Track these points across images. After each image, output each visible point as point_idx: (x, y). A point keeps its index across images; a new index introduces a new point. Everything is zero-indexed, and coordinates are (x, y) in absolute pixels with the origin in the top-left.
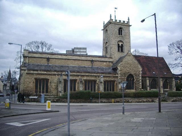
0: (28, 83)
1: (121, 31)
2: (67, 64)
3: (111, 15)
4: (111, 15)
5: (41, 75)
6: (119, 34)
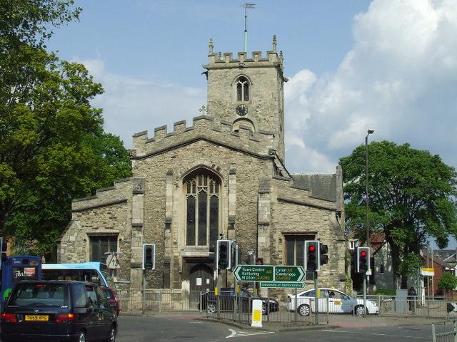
1: (247, 86)
6: (240, 99)
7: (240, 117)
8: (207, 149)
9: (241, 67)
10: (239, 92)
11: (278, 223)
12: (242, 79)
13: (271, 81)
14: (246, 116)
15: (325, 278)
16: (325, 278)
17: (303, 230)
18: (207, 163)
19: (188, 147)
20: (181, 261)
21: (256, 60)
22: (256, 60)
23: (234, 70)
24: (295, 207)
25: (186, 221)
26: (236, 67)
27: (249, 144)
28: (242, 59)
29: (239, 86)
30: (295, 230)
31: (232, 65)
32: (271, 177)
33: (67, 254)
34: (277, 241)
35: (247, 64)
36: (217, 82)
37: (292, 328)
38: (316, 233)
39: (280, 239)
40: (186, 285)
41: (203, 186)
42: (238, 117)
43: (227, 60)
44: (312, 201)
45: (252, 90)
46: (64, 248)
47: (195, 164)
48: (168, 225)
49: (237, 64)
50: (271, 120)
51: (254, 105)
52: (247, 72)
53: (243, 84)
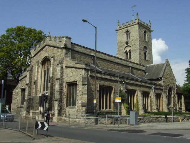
9: (127, 27)
10: (127, 37)
12: (128, 31)
13: (136, 30)
14: (128, 45)
15: (80, 105)
16: (80, 105)
18: (47, 55)
19: (43, 50)
21: (131, 24)
22: (131, 24)
23: (125, 29)
24: (70, 69)
26: (125, 28)
27: (59, 44)
28: (127, 24)
31: (124, 27)
32: (64, 56)
34: (65, 87)
35: (129, 26)
36: (120, 35)
38: (77, 81)
40: (41, 109)
42: (126, 45)
43: (122, 26)
44: (78, 66)
46: (14, 94)
47: (44, 57)
49: (126, 27)
50: (137, 44)
51: (131, 40)
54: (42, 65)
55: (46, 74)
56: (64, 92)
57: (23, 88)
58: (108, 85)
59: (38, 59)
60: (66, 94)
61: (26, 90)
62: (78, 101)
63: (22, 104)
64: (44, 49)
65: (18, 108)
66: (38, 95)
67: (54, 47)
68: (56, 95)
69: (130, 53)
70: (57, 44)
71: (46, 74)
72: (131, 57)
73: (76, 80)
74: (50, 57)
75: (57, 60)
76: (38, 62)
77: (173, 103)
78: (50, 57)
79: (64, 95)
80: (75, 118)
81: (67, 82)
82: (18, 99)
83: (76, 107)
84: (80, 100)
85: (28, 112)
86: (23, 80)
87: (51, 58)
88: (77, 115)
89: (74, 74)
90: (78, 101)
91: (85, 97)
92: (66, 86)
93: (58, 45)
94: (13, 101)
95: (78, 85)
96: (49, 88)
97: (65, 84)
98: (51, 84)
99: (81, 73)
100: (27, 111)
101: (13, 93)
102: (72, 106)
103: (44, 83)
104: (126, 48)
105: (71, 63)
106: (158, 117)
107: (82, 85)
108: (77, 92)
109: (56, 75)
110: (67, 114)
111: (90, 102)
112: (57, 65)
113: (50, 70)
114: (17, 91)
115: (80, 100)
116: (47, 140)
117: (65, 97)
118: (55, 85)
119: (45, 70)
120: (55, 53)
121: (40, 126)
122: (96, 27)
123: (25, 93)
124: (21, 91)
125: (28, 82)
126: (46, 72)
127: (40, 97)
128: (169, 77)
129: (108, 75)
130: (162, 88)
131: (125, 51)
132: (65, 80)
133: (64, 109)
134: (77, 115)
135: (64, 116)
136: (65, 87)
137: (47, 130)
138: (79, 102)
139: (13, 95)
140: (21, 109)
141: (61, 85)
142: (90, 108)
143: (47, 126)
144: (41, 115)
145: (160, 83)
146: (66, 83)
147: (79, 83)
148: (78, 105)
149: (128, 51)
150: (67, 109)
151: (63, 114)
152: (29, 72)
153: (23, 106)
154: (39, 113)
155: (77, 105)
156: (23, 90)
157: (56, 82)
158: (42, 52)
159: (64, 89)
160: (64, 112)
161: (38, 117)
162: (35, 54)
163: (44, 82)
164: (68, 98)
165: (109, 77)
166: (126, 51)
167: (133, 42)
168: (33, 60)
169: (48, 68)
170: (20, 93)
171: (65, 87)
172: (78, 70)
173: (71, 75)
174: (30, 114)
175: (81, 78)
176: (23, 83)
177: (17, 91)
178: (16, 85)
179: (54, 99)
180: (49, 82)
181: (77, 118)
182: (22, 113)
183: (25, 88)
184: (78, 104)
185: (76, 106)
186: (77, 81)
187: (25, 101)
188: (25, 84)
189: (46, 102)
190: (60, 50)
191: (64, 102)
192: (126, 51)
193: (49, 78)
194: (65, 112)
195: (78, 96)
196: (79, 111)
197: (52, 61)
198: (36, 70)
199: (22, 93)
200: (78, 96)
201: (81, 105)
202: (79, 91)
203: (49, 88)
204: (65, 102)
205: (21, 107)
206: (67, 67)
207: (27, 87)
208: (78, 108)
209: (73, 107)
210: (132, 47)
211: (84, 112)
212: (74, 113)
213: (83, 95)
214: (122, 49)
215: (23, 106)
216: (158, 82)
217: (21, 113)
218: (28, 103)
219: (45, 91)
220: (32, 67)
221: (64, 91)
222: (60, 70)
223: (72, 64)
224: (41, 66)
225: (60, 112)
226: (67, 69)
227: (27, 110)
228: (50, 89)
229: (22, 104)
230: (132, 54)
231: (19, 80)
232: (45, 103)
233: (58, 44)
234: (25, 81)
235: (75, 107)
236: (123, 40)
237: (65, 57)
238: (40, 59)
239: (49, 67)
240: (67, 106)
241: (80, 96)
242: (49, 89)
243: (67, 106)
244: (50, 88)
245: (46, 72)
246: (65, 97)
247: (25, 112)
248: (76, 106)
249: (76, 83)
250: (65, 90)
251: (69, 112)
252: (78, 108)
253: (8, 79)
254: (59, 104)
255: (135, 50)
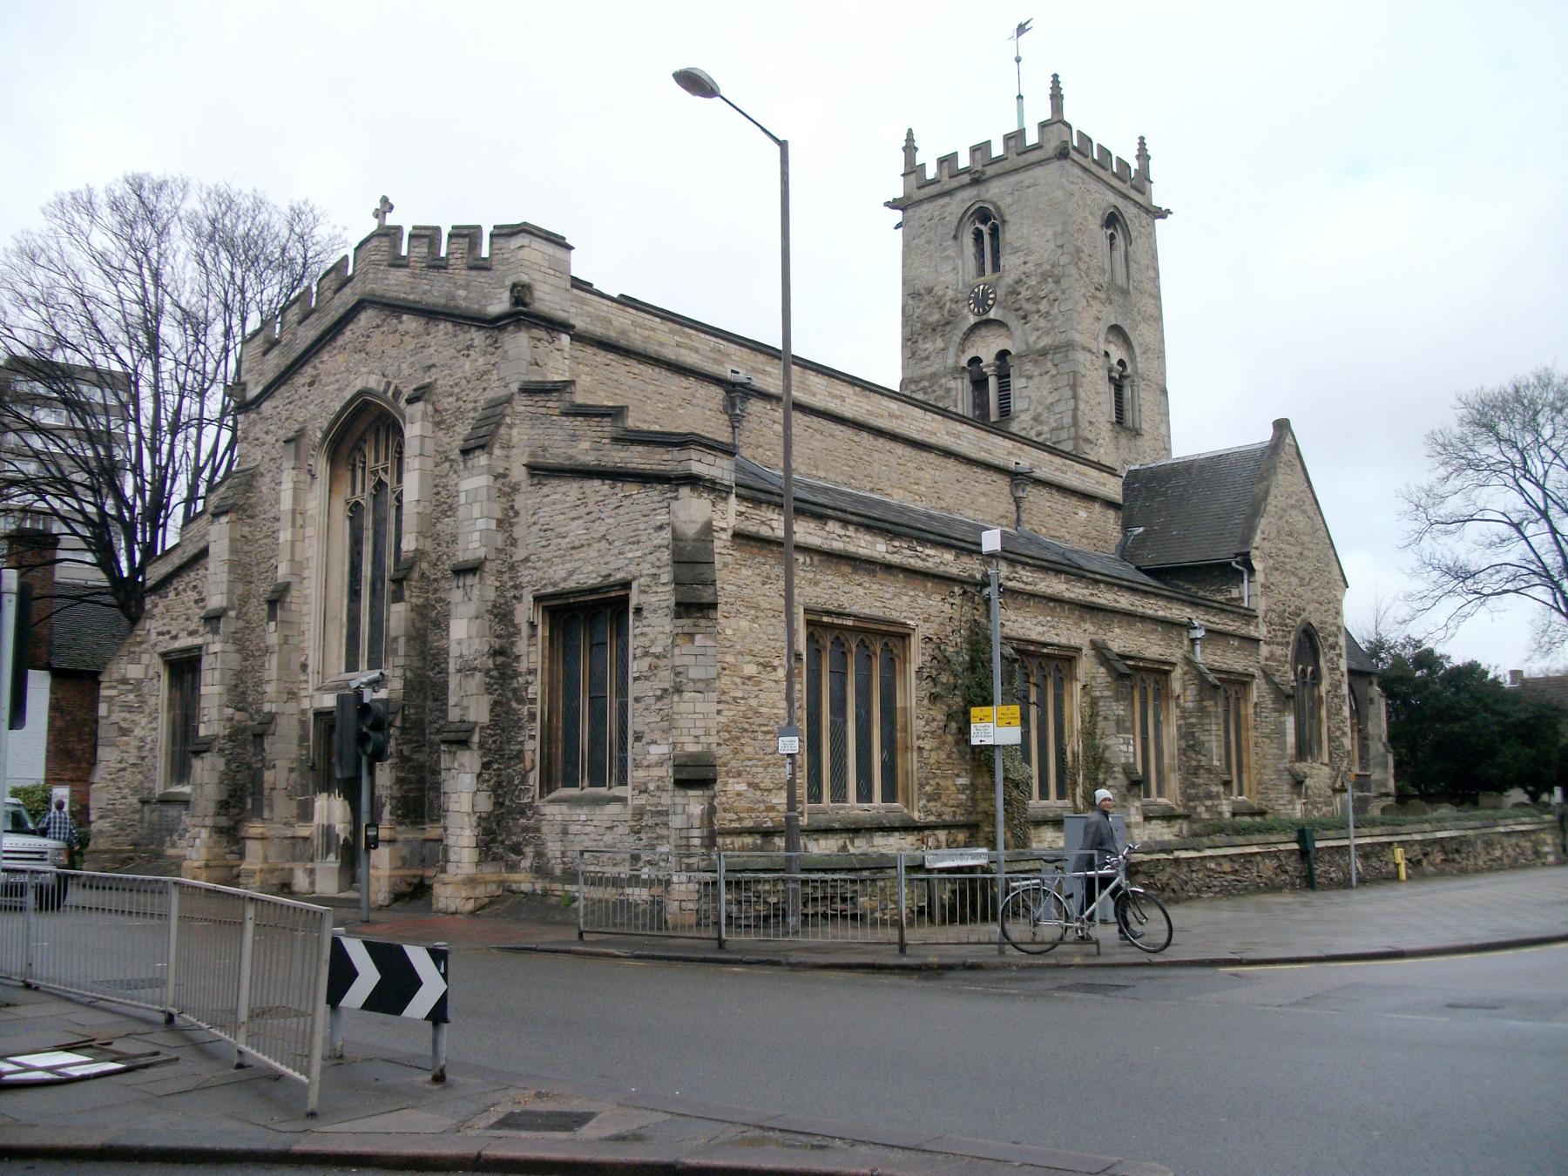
0: (750, 669)
1: (995, 232)
2: (869, 486)
3: (1055, 76)
4: (1055, 76)
5: (847, 569)
6: (981, 271)
7: (977, 319)
8: (377, 335)
11: (527, 560)
12: (983, 215)
14: (992, 315)
17: (593, 581)
18: (374, 382)
19: (340, 341)
20: (311, 715)
25: (346, 589)
26: (963, 187)
27: (466, 287)
29: (978, 236)
30: (571, 584)
33: (117, 716)
36: (923, 240)
37: (573, 948)
38: (626, 585)
39: (533, 626)
41: (380, 466)
42: (972, 319)
45: (1009, 235)
47: (348, 395)
48: (277, 600)
52: (995, 192)
53: (985, 229)
54: (333, 460)
55: (368, 534)
56: (517, 674)
57: (178, 645)
58: (878, 612)
59: (301, 415)
60: (536, 689)
61: (206, 662)
62: (638, 738)
63: (180, 771)
64: (349, 334)
65: (144, 802)
66: (306, 704)
67: (431, 314)
68: (452, 700)
69: (1004, 377)
70: (459, 287)
71: (368, 534)
72: (1017, 405)
73: (619, 576)
74: (397, 394)
75: (459, 414)
76: (294, 440)
77: (1330, 740)
78: (397, 394)
79: (521, 701)
80: (616, 882)
81: (550, 590)
82: (142, 740)
83: (626, 791)
84: (657, 736)
85: (231, 836)
86: (179, 584)
87: (410, 401)
88: (635, 858)
89: (600, 528)
90: (638, 738)
91: (700, 707)
92: (539, 620)
93: (464, 299)
94: (104, 753)
95: (638, 611)
96: (396, 639)
97: (525, 611)
98: (416, 609)
99: (662, 518)
100: (219, 830)
101: (104, 693)
102: (591, 785)
103: (350, 611)
104: (974, 338)
105: (574, 437)
106: (1255, 849)
107: (678, 616)
108: (635, 668)
109: (454, 539)
110: (553, 848)
111: (735, 752)
112: (455, 454)
113: (399, 499)
114: (134, 671)
115: (657, 736)
116: (450, 1121)
117: (532, 716)
118: (447, 617)
119: (357, 504)
120: (435, 360)
121: (368, 976)
122: (783, 145)
123: (195, 687)
124: (165, 678)
125: (216, 601)
126: (368, 521)
127: (320, 714)
128: (1299, 549)
129: (940, 535)
130: (1251, 631)
131: (964, 362)
132: (525, 575)
133: (522, 813)
134: (635, 858)
135: (526, 863)
136: (533, 635)
137: (438, 1014)
138: (653, 749)
139: (103, 709)
140: (172, 812)
141: (501, 614)
142: (739, 794)
143: (432, 987)
144: (333, 861)
145: (1235, 594)
146: (538, 599)
147: (643, 598)
148: (641, 773)
149: (988, 355)
150: (553, 812)
151: (517, 849)
152: (224, 519)
153: (187, 789)
154: (318, 841)
155: (635, 775)
156: (183, 668)
157: (456, 596)
158: (331, 362)
159: (522, 646)
160: (526, 829)
161: (311, 872)
162: (270, 376)
163: (354, 594)
164: (559, 723)
165: (878, 548)
166: (975, 361)
167: (1025, 293)
168: (254, 423)
169: (380, 485)
170: (160, 691)
171: (533, 635)
172: (632, 489)
173: (576, 530)
174: (242, 855)
175: (666, 556)
176: (179, 609)
177: (134, 671)
178: (1400, 784)
179: (439, 731)
180: (398, 598)
181: (635, 881)
182: (183, 843)
183: (200, 648)
184: (637, 766)
185: (623, 781)
186: (626, 585)
187: (197, 753)
188: (196, 619)
189: (379, 755)
190: (478, 337)
191: (519, 756)
192: (975, 361)
193: (389, 561)
194: (538, 830)
195: (637, 700)
196: (648, 820)
197: (412, 431)
198: (286, 503)
199: (171, 686)
200: (637, 700)
201: (667, 772)
202: (649, 660)
203: (396, 639)
204: (528, 756)
205: (166, 801)
206: (541, 472)
207: (210, 637)
208: (642, 800)
209: (603, 791)
210: (1018, 333)
211: (696, 833)
212: (608, 838)
213: (687, 696)
214: (940, 344)
215: (187, 789)
216: (1220, 591)
217: (174, 845)
218: (228, 763)
219: (363, 664)
220: (253, 476)
221: (523, 666)
222: (483, 494)
223: (585, 445)
224: (322, 466)
225: (488, 832)
226: (545, 490)
227: (224, 821)
228: (402, 650)
229: (180, 771)
230: (1017, 383)
231: (149, 583)
232: (364, 759)
233: (462, 293)
234: (194, 596)
235: (618, 791)
236: (949, 278)
237: (523, 390)
238: (314, 417)
239: (386, 479)
240: (547, 784)
241: (659, 698)
242: (395, 652)
243: (547, 784)
244: (402, 640)
245: (368, 521)
246: (532, 716)
247: (205, 834)
248: (623, 781)
249: (625, 600)
250: (532, 654)
251: (565, 832)
252: (642, 800)
253: (796, 480)
254: (486, 766)
255: (1044, 353)
